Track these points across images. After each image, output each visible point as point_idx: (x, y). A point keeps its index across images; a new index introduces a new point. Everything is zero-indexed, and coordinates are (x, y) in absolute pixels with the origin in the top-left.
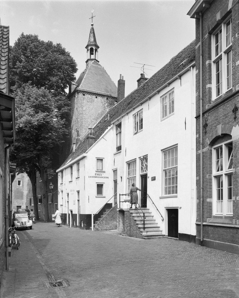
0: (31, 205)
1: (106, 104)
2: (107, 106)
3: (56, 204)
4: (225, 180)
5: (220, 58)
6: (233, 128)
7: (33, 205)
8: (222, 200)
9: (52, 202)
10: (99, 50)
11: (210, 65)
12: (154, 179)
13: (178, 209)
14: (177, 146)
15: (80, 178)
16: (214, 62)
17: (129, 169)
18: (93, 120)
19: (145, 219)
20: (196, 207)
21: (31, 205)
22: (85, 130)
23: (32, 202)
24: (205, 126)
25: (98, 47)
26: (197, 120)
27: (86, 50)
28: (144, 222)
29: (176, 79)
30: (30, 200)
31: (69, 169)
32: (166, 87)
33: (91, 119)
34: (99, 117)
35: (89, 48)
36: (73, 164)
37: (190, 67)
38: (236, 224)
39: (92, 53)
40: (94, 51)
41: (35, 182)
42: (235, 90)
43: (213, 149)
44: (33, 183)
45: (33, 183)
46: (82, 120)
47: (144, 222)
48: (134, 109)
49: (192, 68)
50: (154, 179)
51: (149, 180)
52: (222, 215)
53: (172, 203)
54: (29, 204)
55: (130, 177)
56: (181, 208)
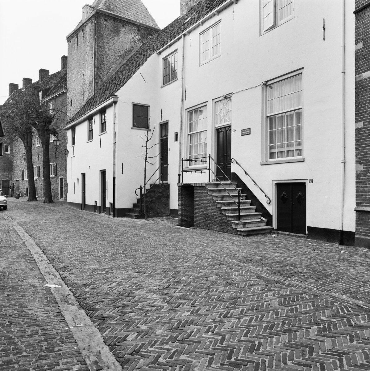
0: (24, 179)
1: (137, 37)
2: (139, 40)
3: (61, 178)
7: (26, 179)
9: (56, 175)
13: (305, 183)
14: (302, 73)
15: (304, 68)
17: (191, 120)
18: (118, 58)
20: (99, 194)
21: (23, 179)
22: (107, 71)
23: (35, 174)
26: (357, 19)
28: (239, 206)
30: (22, 172)
33: (116, 55)
34: (127, 54)
41: (30, 147)
44: (28, 147)
45: (28, 147)
46: (102, 56)
47: (239, 206)
48: (203, 23)
50: (246, 132)
54: (21, 178)
56: (312, 181)
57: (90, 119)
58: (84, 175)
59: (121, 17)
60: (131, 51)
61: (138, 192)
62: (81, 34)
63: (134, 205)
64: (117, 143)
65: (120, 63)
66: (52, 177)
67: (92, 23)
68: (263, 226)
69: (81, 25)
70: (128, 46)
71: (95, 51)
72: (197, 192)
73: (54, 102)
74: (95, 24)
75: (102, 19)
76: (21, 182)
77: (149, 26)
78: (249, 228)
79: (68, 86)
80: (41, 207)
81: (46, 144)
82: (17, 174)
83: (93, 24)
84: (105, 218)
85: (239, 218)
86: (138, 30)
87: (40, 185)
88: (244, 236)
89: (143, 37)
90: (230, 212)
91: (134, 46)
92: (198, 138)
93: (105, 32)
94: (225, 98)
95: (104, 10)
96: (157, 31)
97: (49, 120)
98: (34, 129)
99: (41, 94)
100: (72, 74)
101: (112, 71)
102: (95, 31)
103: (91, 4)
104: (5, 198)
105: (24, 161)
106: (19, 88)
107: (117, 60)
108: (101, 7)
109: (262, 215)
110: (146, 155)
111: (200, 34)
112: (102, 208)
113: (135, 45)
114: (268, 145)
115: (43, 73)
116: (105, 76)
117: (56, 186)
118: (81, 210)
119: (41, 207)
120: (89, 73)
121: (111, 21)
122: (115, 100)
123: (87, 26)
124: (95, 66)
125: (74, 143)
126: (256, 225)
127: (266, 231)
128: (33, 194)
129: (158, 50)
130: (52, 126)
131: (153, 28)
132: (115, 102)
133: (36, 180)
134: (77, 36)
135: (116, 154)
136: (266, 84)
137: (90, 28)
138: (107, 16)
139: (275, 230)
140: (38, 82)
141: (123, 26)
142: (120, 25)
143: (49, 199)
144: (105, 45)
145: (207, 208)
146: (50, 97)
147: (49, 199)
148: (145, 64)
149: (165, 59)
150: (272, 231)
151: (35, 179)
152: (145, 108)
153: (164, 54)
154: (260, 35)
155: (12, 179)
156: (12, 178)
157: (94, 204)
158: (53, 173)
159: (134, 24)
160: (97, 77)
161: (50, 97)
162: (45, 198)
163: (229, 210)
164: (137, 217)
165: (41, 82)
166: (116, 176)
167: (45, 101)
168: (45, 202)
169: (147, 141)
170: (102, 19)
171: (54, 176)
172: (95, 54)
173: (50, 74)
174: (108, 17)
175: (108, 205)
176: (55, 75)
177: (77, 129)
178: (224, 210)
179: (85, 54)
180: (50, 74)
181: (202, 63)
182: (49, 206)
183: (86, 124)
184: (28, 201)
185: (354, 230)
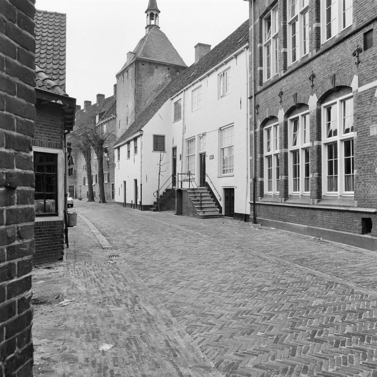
1: (168, 75)
2: (169, 77)
4: (341, 149)
5: (296, 19)
6: (310, 97)
7: (87, 184)
8: (335, 174)
9: (109, 181)
10: (160, 15)
11: (261, 48)
12: (212, 157)
13: (234, 189)
16: (265, 45)
19: (202, 199)
21: (85, 184)
24: (257, 107)
25: (159, 12)
27: (146, 15)
29: (232, 58)
31: (126, 146)
32: (222, 65)
33: (151, 90)
35: (149, 13)
36: (131, 140)
37: (244, 48)
38: (282, 202)
39: (152, 18)
40: (155, 16)
41: (90, 160)
42: (281, 75)
43: (264, 130)
48: (193, 85)
49: (246, 49)
51: (207, 159)
52: (337, 195)
53: (228, 182)
54: (83, 184)
55: (189, 155)
57: (128, 143)
58: (125, 182)
59: (154, 61)
60: (163, 85)
61: (156, 194)
62: (126, 74)
63: (155, 203)
64: (143, 162)
65: (154, 96)
66: (106, 184)
67: (133, 67)
68: (217, 213)
69: (126, 67)
70: (160, 82)
71: (135, 89)
72: (184, 194)
73: (107, 124)
74: (135, 68)
75: (140, 64)
76: (83, 187)
77: (177, 65)
78: (206, 214)
79: (117, 113)
80: (96, 205)
81: (101, 159)
82: (80, 180)
83: (134, 68)
84: (137, 212)
85: (201, 208)
86: (169, 69)
87: (96, 189)
88: (202, 218)
89: (172, 74)
90: (197, 205)
91: (165, 82)
92: (188, 159)
93: (143, 73)
94: (203, 135)
95: (142, 57)
96: (184, 68)
97: (102, 142)
98: (92, 147)
99: (97, 117)
100: (120, 104)
101: (148, 103)
102: (135, 74)
103: (132, 51)
104: (72, 199)
105: (85, 170)
106: (81, 109)
107: (152, 94)
108: (139, 55)
109: (218, 208)
110: (160, 170)
111: (192, 91)
112: (134, 206)
113: (166, 81)
114: (222, 165)
115: (100, 97)
116: (143, 107)
117: (107, 190)
118: (141, 210)
119: (96, 205)
120: (131, 104)
121: (147, 65)
122: (141, 133)
123: (130, 69)
124: (135, 100)
125: (119, 159)
126: (212, 213)
127: (217, 216)
128: (91, 197)
129: (171, 96)
130: (105, 146)
131: (181, 66)
132: (142, 135)
133: (94, 185)
134: (123, 76)
135: (142, 169)
136: (220, 129)
137: (131, 70)
138: (143, 61)
139: (224, 216)
140: (96, 104)
141: (157, 67)
142: (154, 67)
143: (103, 200)
144: (143, 83)
145: (187, 204)
146: (104, 121)
147: (103, 200)
148: (162, 107)
149: (176, 103)
150: (221, 216)
151: (93, 185)
152: (163, 137)
153: (175, 100)
154: (218, 99)
155: (76, 184)
156: (76, 183)
157: (131, 203)
158: (106, 180)
159: (165, 65)
160: (137, 108)
161: (104, 121)
162: (100, 199)
163: (196, 204)
164: (154, 211)
165: (98, 105)
166: (142, 184)
167: (100, 123)
168: (100, 202)
169: (160, 161)
170: (140, 64)
171: (107, 182)
172: (135, 91)
173: (106, 98)
174: (144, 62)
175: (138, 203)
176: (109, 99)
177: (121, 148)
178: (194, 204)
179: (129, 90)
180: (106, 98)
181: (194, 110)
182: (103, 205)
183: (126, 146)
184: (88, 201)
185: (249, 214)
